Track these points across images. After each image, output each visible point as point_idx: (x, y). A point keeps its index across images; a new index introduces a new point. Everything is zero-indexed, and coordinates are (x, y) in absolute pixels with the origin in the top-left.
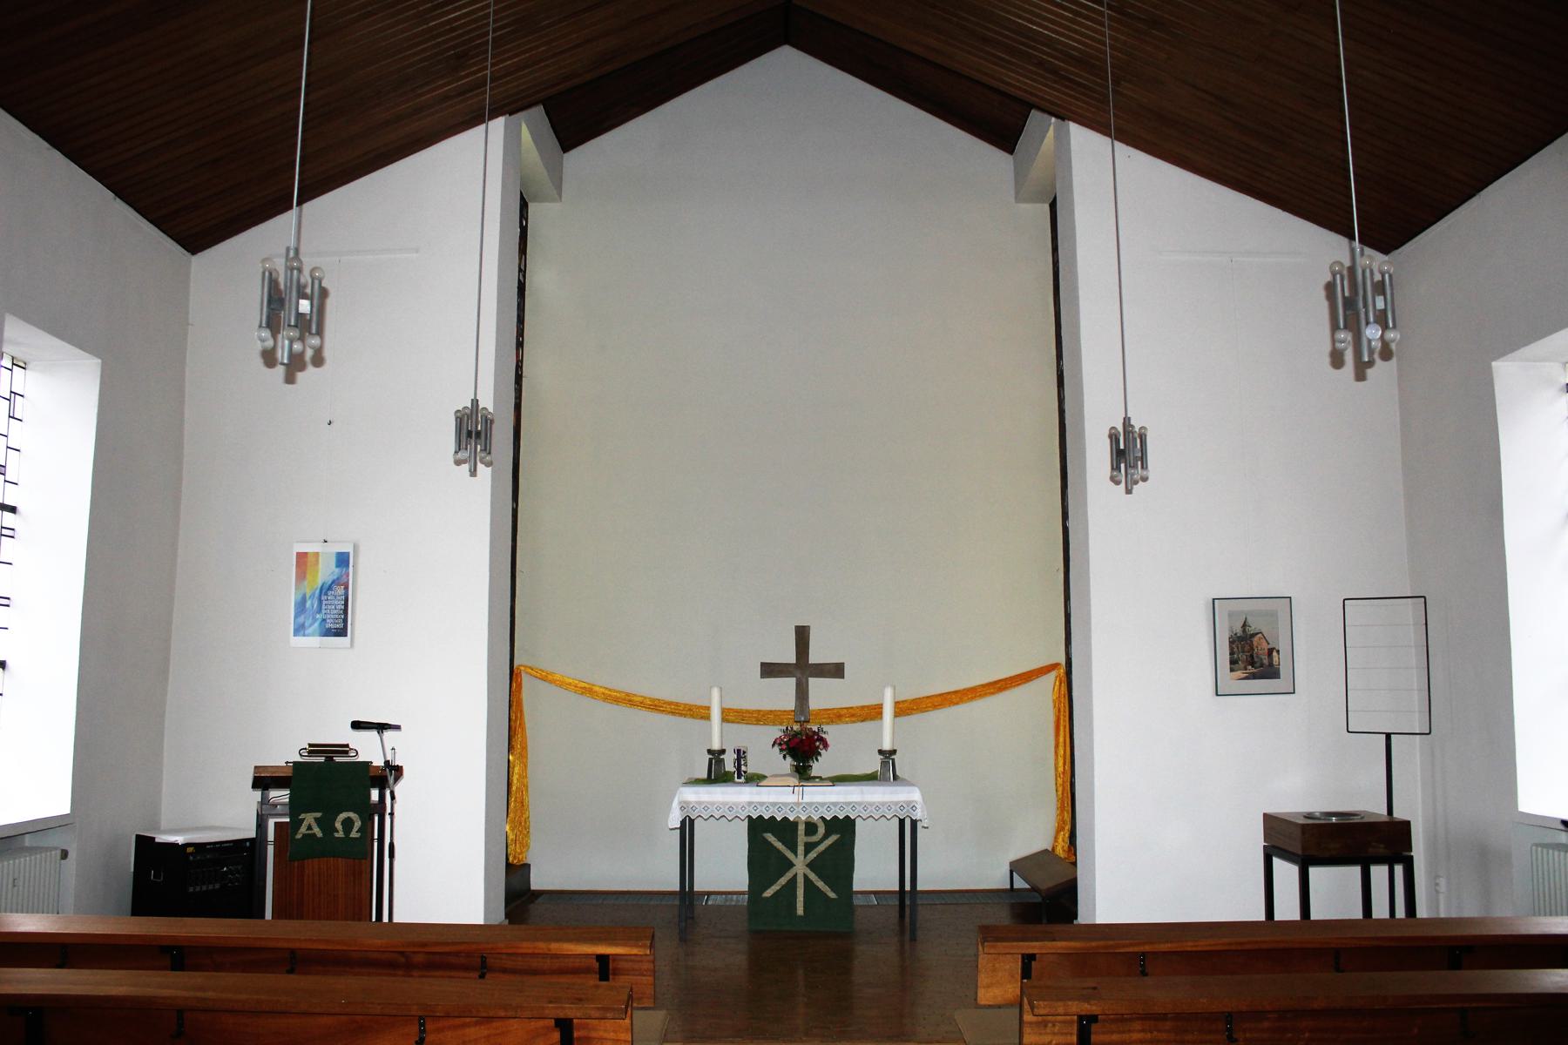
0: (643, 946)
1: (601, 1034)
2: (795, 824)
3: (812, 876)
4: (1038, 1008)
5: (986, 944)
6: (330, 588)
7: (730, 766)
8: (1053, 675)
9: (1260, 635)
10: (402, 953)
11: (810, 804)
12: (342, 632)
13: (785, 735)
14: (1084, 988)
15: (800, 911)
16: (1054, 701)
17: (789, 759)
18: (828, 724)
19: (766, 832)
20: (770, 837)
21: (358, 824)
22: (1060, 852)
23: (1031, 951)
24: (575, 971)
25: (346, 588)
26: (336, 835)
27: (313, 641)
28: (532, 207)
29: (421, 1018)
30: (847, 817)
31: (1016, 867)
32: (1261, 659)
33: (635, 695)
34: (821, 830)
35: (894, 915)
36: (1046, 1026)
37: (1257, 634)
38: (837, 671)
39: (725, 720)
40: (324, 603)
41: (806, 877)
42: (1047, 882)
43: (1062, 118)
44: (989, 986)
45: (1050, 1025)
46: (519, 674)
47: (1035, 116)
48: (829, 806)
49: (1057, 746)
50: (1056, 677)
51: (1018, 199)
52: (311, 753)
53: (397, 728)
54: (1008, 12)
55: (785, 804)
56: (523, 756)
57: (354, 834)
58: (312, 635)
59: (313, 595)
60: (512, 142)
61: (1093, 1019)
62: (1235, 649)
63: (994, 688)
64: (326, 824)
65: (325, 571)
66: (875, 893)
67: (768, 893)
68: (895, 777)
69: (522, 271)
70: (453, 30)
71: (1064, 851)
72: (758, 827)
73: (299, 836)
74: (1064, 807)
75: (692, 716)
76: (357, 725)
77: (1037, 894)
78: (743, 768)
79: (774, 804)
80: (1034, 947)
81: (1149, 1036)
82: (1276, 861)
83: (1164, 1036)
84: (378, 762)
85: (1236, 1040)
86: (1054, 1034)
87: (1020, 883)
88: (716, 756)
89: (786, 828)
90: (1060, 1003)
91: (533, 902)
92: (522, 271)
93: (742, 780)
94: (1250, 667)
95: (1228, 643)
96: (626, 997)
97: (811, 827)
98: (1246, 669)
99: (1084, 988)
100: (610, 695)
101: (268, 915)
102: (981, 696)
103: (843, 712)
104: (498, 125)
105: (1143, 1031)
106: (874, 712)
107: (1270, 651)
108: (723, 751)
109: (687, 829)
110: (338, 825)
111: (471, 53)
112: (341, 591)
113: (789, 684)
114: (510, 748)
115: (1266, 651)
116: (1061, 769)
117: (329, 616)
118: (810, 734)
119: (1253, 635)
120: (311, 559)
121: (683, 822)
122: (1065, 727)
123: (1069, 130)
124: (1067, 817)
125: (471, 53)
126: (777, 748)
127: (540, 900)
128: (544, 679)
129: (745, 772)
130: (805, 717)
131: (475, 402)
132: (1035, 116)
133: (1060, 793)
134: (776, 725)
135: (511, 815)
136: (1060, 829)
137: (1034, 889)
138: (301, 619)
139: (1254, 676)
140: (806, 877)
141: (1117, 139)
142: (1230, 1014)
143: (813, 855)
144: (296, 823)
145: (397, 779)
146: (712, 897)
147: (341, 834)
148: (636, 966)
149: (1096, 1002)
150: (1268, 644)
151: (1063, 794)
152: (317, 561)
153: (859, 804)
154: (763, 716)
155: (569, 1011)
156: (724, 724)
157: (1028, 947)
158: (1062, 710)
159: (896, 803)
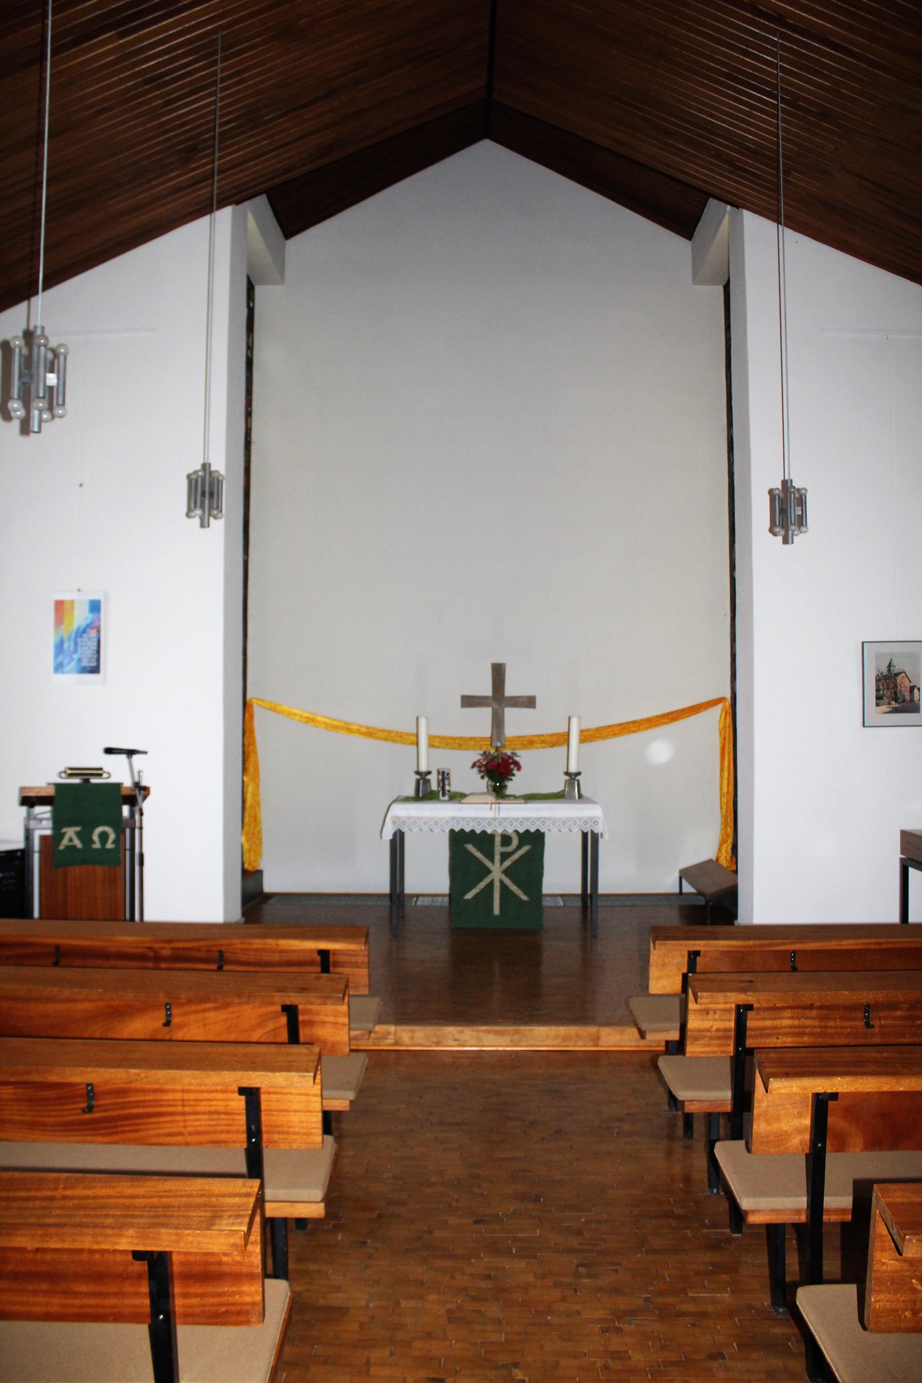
0: (360, 943)
1: (322, 1018)
2: (492, 837)
3: (507, 881)
4: (701, 998)
5: (657, 942)
6: (84, 631)
7: (434, 786)
8: (719, 707)
9: (903, 674)
10: (151, 948)
11: (505, 819)
12: (95, 670)
13: (484, 759)
14: (742, 982)
15: (497, 911)
16: (720, 730)
17: (486, 779)
18: (521, 749)
19: (468, 842)
20: (470, 848)
21: (112, 837)
22: (724, 862)
23: (696, 948)
24: (300, 964)
25: (99, 631)
26: (94, 846)
27: (72, 680)
28: (259, 290)
29: (167, 1004)
30: (538, 831)
31: (685, 874)
32: (904, 695)
33: (352, 724)
34: (515, 842)
35: (577, 915)
36: (708, 1013)
37: (901, 673)
38: (530, 702)
39: (431, 745)
40: (80, 644)
41: (501, 882)
42: (712, 887)
43: (736, 206)
44: (659, 978)
45: (711, 1012)
46: (251, 706)
47: (712, 203)
48: (522, 821)
49: (722, 770)
50: (722, 710)
51: (695, 280)
52: (71, 775)
53: (145, 753)
54: (690, 107)
55: (484, 819)
56: (256, 778)
57: (110, 845)
58: (70, 672)
59: (69, 638)
60: (239, 230)
61: (750, 1007)
62: (881, 687)
63: (668, 719)
64: (85, 836)
65: (80, 617)
66: (562, 896)
67: (469, 896)
68: (580, 796)
69: (250, 348)
70: (183, 125)
71: (727, 861)
72: (458, 839)
73: (62, 847)
74: (728, 823)
75: (403, 743)
76: (109, 751)
77: (702, 898)
78: (447, 788)
79: (474, 819)
80: (699, 945)
81: (796, 1022)
82: (912, 872)
83: (809, 1022)
84: (127, 783)
85: (873, 1026)
86: (715, 1020)
87: (688, 888)
88: (422, 777)
89: (484, 840)
90: (720, 994)
91: (265, 903)
92: (250, 348)
93: (446, 798)
94: (894, 702)
95: (875, 681)
96: (343, 987)
97: (506, 840)
98: (890, 704)
99: (742, 982)
100: (331, 724)
101: (36, 914)
102: (656, 725)
103: (534, 739)
104: (225, 216)
105: (792, 1018)
106: (563, 739)
107: (912, 689)
108: (429, 773)
109: (397, 844)
110: (95, 838)
111: (200, 147)
112: (93, 633)
113: (485, 714)
114: (245, 770)
115: (908, 689)
116: (725, 790)
117: (83, 656)
118: (506, 758)
119: (897, 674)
120: (67, 606)
121: (395, 835)
122: (729, 753)
123: (742, 214)
124: (730, 831)
125: (200, 147)
126: (476, 770)
127: (272, 901)
128: (274, 710)
129: (449, 791)
130: (501, 743)
131: (205, 466)
132: (712, 203)
133: (724, 810)
134: (476, 750)
135: (246, 828)
136: (723, 842)
137: (700, 893)
138: (60, 659)
139: (895, 711)
140: (501, 882)
141: (786, 225)
142: (868, 1005)
143: (507, 863)
144: (58, 835)
145: (145, 798)
146: (420, 899)
147: (97, 845)
148: (353, 959)
149: (752, 993)
150: (910, 682)
151: (726, 811)
152: (72, 608)
153: (549, 819)
154: (465, 742)
155: (293, 999)
156: (432, 749)
157: (694, 945)
158: (727, 738)
159: (580, 819)
